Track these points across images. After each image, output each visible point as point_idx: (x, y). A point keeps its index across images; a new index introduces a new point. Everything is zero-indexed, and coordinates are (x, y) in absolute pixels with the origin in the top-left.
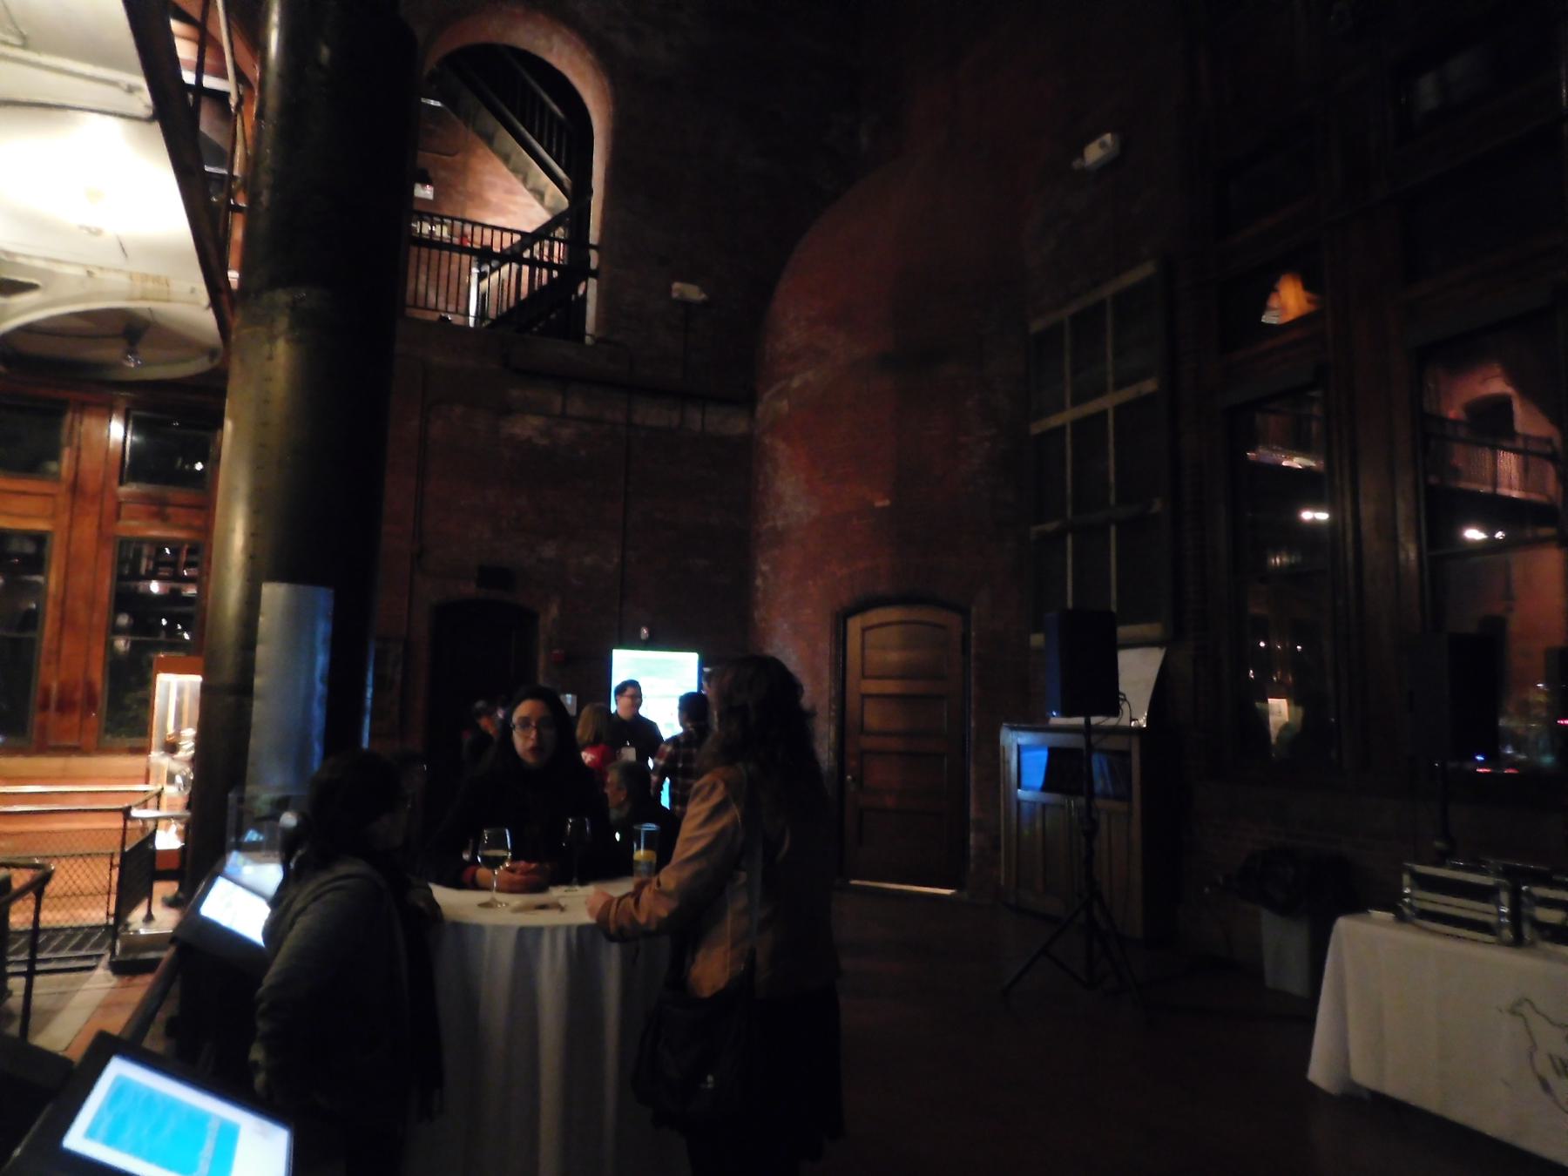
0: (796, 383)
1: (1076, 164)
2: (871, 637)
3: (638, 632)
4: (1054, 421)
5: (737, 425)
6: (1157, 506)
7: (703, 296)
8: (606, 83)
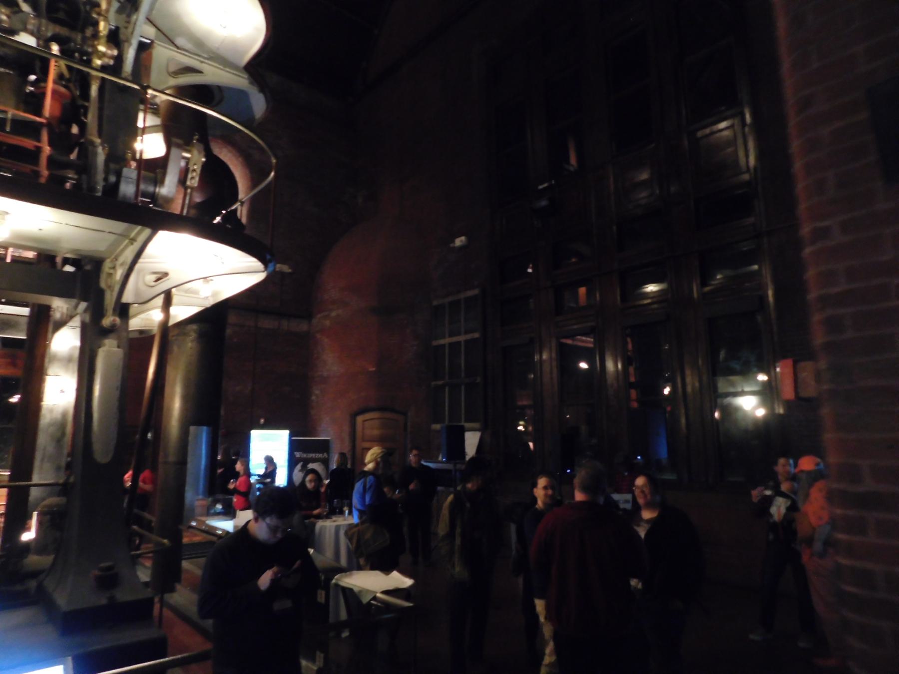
0: (333, 314)
1: (452, 245)
2: (367, 424)
3: (259, 421)
4: (442, 342)
5: (303, 327)
6: (479, 380)
7: (290, 271)
8: (248, 172)
